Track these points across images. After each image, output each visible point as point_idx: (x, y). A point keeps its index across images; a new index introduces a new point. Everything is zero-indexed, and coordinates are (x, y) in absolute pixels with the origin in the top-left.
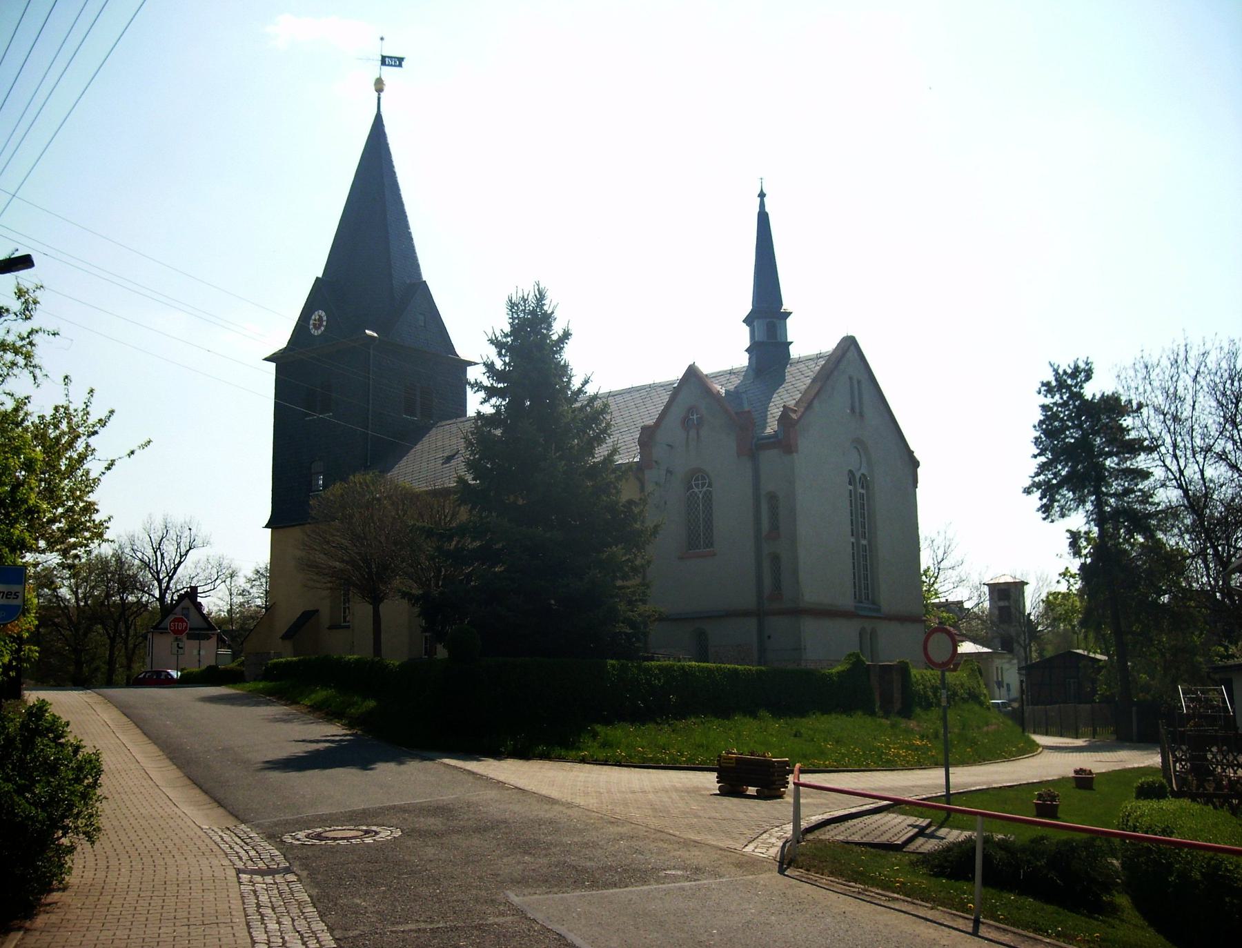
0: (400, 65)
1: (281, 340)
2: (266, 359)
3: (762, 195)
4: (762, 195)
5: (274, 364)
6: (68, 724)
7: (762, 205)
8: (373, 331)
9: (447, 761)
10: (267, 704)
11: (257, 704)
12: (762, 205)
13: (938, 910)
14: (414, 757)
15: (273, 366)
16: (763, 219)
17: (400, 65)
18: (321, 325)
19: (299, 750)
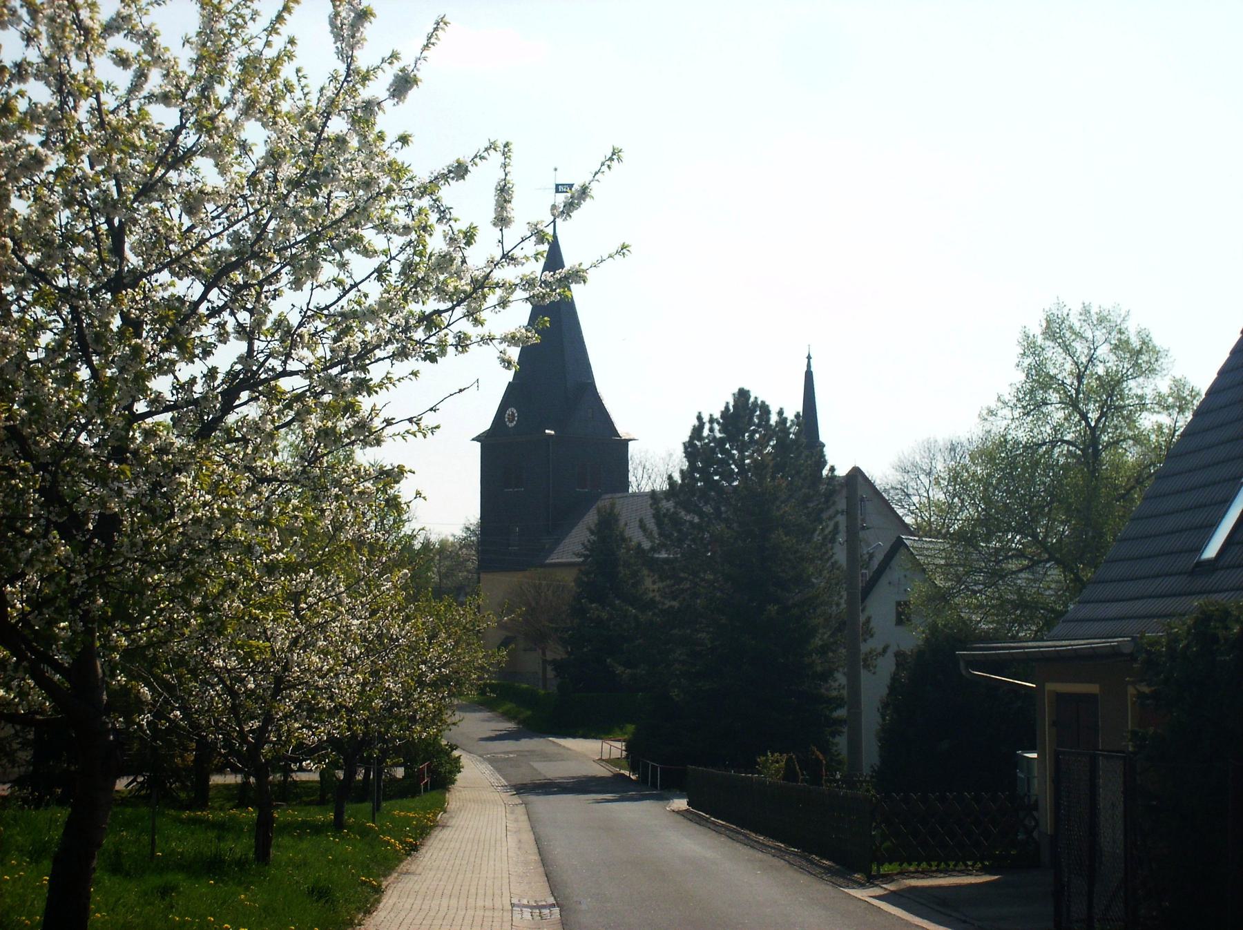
0: (557, 186)
1: (485, 424)
2: (473, 440)
3: (809, 358)
4: (809, 358)
5: (479, 444)
6: (647, 452)
7: (809, 365)
8: (551, 430)
9: (550, 739)
10: (480, 711)
11: (474, 711)
12: (809, 365)
13: (882, 887)
14: (537, 737)
15: (479, 444)
16: (809, 376)
17: (557, 186)
18: (513, 420)
19: (493, 734)
